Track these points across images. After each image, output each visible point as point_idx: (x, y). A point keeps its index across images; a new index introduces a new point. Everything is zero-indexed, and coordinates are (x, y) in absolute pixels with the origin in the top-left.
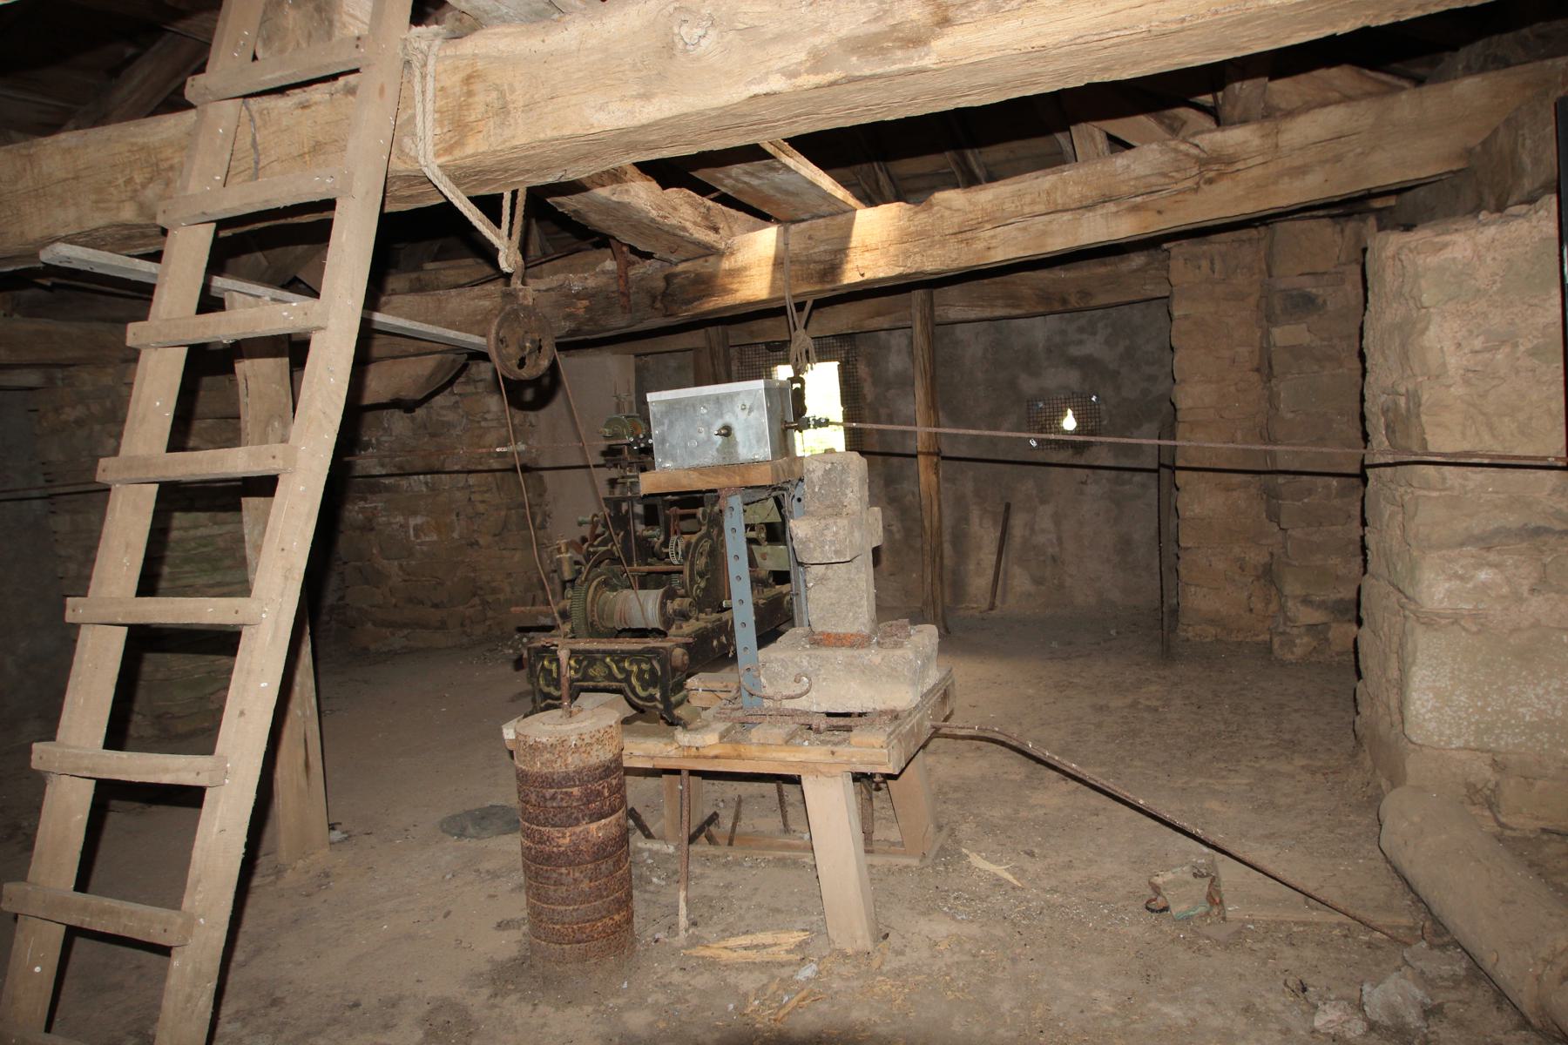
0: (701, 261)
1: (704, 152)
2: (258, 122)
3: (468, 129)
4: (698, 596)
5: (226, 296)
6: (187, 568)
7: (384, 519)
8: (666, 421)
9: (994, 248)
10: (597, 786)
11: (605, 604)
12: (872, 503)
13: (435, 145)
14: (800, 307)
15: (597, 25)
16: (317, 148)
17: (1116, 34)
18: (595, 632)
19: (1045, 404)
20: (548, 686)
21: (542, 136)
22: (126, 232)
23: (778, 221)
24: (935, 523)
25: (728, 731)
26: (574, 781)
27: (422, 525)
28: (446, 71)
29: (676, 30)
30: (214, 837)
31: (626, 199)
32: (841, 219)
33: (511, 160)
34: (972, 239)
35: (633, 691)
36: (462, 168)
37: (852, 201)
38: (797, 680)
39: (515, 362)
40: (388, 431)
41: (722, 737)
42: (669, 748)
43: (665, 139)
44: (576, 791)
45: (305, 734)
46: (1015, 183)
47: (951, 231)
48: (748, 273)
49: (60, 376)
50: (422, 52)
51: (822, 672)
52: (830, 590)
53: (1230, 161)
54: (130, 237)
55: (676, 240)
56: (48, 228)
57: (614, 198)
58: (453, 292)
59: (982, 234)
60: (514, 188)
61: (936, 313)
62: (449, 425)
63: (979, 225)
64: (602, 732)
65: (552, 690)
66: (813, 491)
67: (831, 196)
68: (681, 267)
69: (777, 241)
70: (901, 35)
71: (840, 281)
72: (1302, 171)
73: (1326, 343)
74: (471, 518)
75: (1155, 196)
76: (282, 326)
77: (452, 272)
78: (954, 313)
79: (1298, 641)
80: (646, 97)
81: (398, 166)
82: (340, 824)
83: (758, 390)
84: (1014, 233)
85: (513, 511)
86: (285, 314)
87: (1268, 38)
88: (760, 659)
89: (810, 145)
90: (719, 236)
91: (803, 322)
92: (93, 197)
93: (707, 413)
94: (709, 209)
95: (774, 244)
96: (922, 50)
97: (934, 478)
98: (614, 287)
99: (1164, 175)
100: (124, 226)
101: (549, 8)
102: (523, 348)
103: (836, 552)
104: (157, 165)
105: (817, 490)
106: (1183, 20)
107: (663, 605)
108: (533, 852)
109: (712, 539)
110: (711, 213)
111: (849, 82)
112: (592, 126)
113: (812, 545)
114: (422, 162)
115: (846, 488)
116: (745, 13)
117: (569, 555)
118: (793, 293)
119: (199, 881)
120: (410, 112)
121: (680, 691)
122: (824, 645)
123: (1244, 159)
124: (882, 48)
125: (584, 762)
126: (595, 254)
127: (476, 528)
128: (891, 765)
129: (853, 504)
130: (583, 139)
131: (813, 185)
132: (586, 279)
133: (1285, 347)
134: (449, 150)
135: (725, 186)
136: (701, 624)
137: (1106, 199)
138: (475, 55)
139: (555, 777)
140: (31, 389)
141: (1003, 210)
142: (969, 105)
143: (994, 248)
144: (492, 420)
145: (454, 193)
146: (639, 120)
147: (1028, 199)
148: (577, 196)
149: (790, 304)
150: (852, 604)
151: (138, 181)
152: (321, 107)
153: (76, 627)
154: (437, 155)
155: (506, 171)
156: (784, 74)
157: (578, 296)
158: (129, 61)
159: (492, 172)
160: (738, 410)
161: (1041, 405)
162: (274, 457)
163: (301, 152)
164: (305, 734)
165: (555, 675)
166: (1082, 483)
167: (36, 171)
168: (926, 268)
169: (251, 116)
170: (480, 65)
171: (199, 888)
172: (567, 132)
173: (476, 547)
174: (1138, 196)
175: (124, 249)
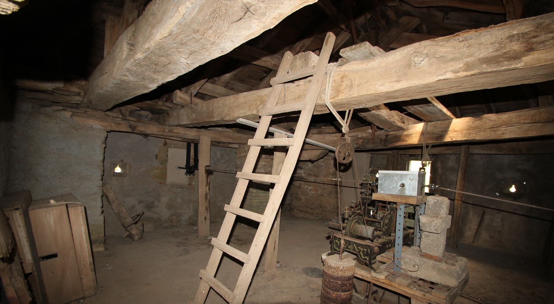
0: (397, 132)
1: (413, 99)
2: (286, 90)
3: (340, 92)
4: (384, 231)
5: (275, 133)
8: (383, 179)
10: (345, 282)
11: (356, 228)
12: (449, 214)
13: (330, 96)
14: (427, 147)
15: (385, 59)
16: (299, 97)
18: (352, 236)
21: (362, 94)
22: (254, 116)
23: (425, 121)
25: (388, 276)
27: (311, 189)
28: (336, 75)
29: (413, 59)
31: (379, 113)
32: (446, 121)
33: (351, 101)
35: (360, 256)
37: (452, 116)
39: (342, 158)
40: (307, 166)
41: (386, 277)
42: (369, 276)
43: (401, 95)
44: (339, 282)
46: (518, 112)
47: (489, 127)
48: (412, 136)
49: (242, 146)
50: (330, 70)
52: (430, 240)
54: (255, 118)
56: (238, 114)
58: (328, 135)
59: (501, 129)
60: (350, 109)
61: (470, 151)
62: (322, 166)
63: (501, 126)
65: (337, 248)
66: (429, 208)
67: (446, 114)
68: (391, 133)
69: (423, 127)
70: (508, 56)
76: (282, 144)
77: (328, 129)
78: (475, 151)
80: (398, 81)
82: (280, 262)
83: (416, 174)
84: (515, 129)
85: (333, 189)
88: (402, 256)
89: (441, 99)
90: (404, 125)
92: (248, 108)
93: (397, 179)
94: (403, 117)
98: (370, 137)
100: (254, 115)
101: (370, 55)
102: (345, 155)
103: (435, 230)
104: (262, 100)
105: (430, 207)
107: (373, 233)
108: (325, 295)
110: (403, 118)
111: (480, 74)
113: (426, 226)
114: (326, 101)
116: (440, 52)
117: (348, 211)
119: (239, 287)
120: (325, 87)
121: (375, 259)
122: (425, 257)
124: (498, 61)
126: (365, 128)
127: (324, 191)
130: (374, 95)
131: (441, 111)
132: (363, 134)
134: (333, 98)
135: (411, 110)
136: (384, 240)
138: (345, 70)
139: (334, 277)
140: (236, 148)
141: (511, 121)
146: (394, 89)
147: (523, 118)
148: (367, 113)
149: (424, 146)
150: (437, 246)
151: (258, 104)
153: (226, 212)
154: (330, 99)
155: (349, 104)
156: (453, 72)
157: (360, 138)
158: (264, 77)
159: (345, 104)
160: (408, 180)
162: (275, 179)
163: (295, 98)
167: (238, 101)
171: (238, 289)
172: (370, 93)
173: (323, 196)
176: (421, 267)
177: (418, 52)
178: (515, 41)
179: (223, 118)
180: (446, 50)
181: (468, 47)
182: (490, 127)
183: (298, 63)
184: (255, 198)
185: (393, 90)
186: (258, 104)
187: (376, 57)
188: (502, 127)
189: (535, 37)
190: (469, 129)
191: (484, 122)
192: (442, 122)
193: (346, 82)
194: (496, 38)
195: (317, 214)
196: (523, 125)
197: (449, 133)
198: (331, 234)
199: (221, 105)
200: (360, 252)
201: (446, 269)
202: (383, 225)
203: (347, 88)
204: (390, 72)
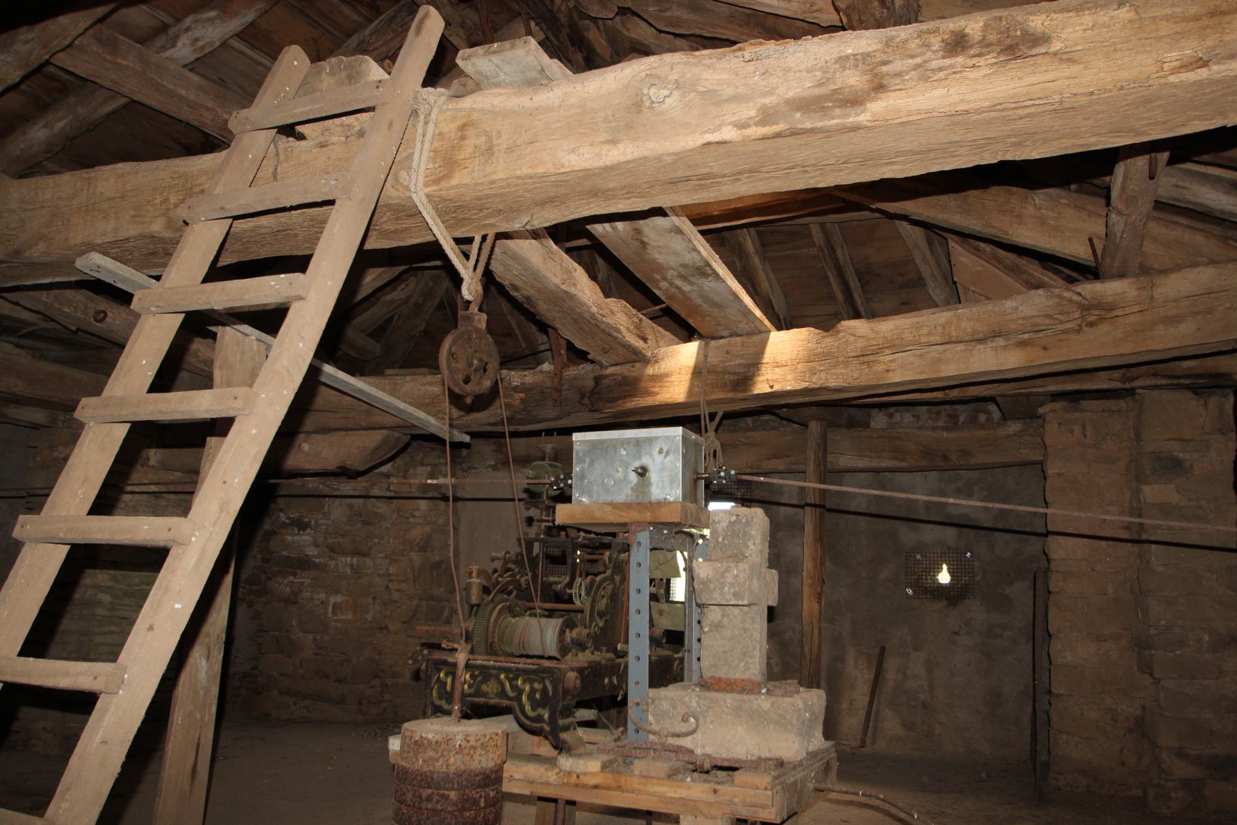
0: (628, 366)
2: (282, 157)
4: (595, 633)
6: (127, 601)
7: (309, 594)
8: (588, 460)
9: (893, 370)
10: (474, 794)
11: (506, 627)
13: (425, 177)
14: (712, 416)
15: (579, 87)
17: (1031, 103)
18: (491, 650)
19: (922, 557)
20: (440, 699)
21: (518, 173)
23: (701, 337)
24: (815, 650)
25: (611, 762)
26: (453, 783)
28: (445, 120)
29: (645, 91)
30: (94, 746)
32: (756, 338)
33: (488, 197)
34: (873, 362)
36: (445, 200)
38: (685, 720)
39: (460, 377)
42: (550, 774)
45: (199, 739)
47: (854, 354)
48: (668, 379)
49: (62, 418)
51: (711, 713)
53: (1110, 308)
55: (609, 337)
56: (88, 236)
57: (564, 287)
59: (881, 358)
63: (879, 351)
64: (488, 737)
65: (443, 703)
66: (717, 541)
68: (610, 370)
69: (698, 354)
70: (840, 97)
71: (751, 391)
72: (1176, 320)
73: (1194, 503)
74: (385, 604)
75: (1041, 334)
79: (1173, 795)
80: (613, 142)
81: (391, 193)
85: (424, 602)
86: (273, 283)
87: (1165, 122)
91: (714, 427)
92: (132, 213)
95: (695, 355)
96: (859, 109)
97: (816, 606)
98: (549, 384)
99: (1050, 317)
102: (470, 365)
104: (191, 189)
105: (720, 540)
106: (1092, 94)
107: (562, 633)
109: (615, 585)
112: (563, 166)
113: (712, 586)
115: (749, 540)
116: (706, 80)
118: (707, 399)
119: (69, 789)
120: (410, 151)
123: (1123, 307)
125: (465, 765)
127: (388, 614)
128: (773, 811)
129: (754, 555)
132: (525, 376)
133: (1155, 504)
134: (437, 181)
135: (660, 289)
137: (995, 335)
138: (473, 109)
139: (435, 776)
142: (892, 176)
143: (893, 370)
144: (419, 517)
145: (434, 221)
146: (604, 162)
147: (925, 331)
151: (172, 201)
152: (336, 147)
154: (426, 185)
157: (516, 389)
160: (655, 453)
161: (918, 557)
164: (199, 739)
165: (448, 688)
166: (955, 633)
167: (91, 190)
168: (829, 385)
169: (277, 152)
170: (475, 116)
171: (67, 796)
172: (540, 170)
173: (385, 631)
174: (1025, 333)
175: (147, 267)
176: (705, 717)
177: (657, 77)
178: (850, 69)
179: (17, 253)
180: (717, 77)
181: (763, 74)
182: (857, 354)
183: (325, 84)
184: (106, 629)
185: (601, 164)
186: (172, 201)
187: (554, 83)
188: (883, 352)
189: (885, 63)
190: (812, 359)
191: (844, 340)
192: (745, 339)
193: (474, 141)
194: (816, 59)
195: (360, 703)
196: (928, 349)
197: (763, 369)
198: (422, 655)
199: (13, 206)
200: (521, 699)
201: (768, 710)
202: (590, 616)
203: (477, 155)
204: (591, 119)
